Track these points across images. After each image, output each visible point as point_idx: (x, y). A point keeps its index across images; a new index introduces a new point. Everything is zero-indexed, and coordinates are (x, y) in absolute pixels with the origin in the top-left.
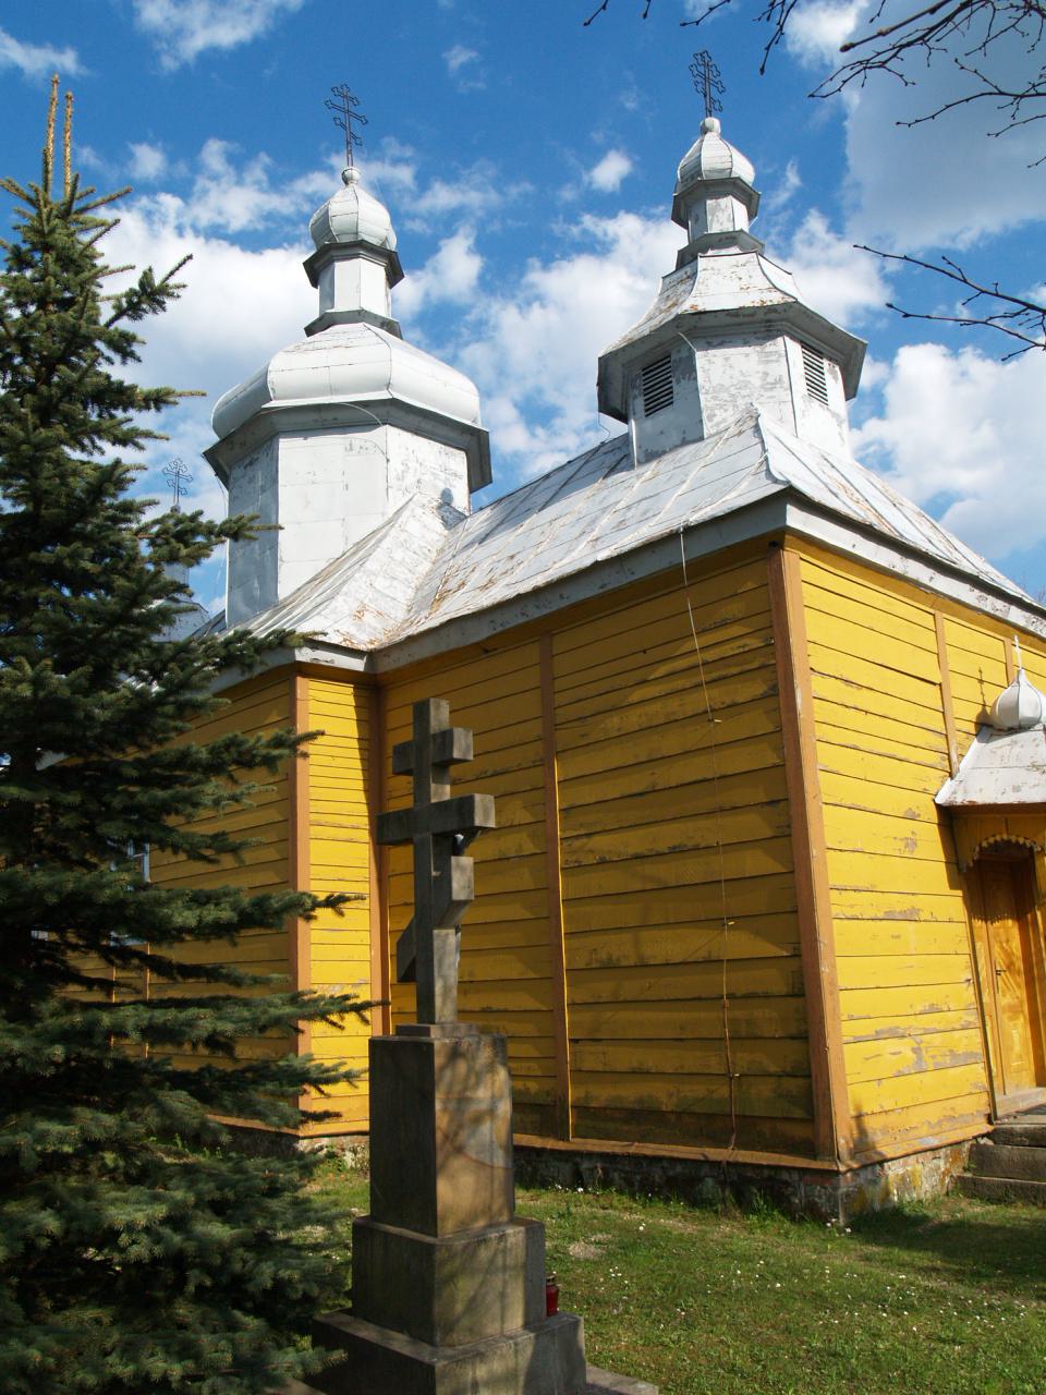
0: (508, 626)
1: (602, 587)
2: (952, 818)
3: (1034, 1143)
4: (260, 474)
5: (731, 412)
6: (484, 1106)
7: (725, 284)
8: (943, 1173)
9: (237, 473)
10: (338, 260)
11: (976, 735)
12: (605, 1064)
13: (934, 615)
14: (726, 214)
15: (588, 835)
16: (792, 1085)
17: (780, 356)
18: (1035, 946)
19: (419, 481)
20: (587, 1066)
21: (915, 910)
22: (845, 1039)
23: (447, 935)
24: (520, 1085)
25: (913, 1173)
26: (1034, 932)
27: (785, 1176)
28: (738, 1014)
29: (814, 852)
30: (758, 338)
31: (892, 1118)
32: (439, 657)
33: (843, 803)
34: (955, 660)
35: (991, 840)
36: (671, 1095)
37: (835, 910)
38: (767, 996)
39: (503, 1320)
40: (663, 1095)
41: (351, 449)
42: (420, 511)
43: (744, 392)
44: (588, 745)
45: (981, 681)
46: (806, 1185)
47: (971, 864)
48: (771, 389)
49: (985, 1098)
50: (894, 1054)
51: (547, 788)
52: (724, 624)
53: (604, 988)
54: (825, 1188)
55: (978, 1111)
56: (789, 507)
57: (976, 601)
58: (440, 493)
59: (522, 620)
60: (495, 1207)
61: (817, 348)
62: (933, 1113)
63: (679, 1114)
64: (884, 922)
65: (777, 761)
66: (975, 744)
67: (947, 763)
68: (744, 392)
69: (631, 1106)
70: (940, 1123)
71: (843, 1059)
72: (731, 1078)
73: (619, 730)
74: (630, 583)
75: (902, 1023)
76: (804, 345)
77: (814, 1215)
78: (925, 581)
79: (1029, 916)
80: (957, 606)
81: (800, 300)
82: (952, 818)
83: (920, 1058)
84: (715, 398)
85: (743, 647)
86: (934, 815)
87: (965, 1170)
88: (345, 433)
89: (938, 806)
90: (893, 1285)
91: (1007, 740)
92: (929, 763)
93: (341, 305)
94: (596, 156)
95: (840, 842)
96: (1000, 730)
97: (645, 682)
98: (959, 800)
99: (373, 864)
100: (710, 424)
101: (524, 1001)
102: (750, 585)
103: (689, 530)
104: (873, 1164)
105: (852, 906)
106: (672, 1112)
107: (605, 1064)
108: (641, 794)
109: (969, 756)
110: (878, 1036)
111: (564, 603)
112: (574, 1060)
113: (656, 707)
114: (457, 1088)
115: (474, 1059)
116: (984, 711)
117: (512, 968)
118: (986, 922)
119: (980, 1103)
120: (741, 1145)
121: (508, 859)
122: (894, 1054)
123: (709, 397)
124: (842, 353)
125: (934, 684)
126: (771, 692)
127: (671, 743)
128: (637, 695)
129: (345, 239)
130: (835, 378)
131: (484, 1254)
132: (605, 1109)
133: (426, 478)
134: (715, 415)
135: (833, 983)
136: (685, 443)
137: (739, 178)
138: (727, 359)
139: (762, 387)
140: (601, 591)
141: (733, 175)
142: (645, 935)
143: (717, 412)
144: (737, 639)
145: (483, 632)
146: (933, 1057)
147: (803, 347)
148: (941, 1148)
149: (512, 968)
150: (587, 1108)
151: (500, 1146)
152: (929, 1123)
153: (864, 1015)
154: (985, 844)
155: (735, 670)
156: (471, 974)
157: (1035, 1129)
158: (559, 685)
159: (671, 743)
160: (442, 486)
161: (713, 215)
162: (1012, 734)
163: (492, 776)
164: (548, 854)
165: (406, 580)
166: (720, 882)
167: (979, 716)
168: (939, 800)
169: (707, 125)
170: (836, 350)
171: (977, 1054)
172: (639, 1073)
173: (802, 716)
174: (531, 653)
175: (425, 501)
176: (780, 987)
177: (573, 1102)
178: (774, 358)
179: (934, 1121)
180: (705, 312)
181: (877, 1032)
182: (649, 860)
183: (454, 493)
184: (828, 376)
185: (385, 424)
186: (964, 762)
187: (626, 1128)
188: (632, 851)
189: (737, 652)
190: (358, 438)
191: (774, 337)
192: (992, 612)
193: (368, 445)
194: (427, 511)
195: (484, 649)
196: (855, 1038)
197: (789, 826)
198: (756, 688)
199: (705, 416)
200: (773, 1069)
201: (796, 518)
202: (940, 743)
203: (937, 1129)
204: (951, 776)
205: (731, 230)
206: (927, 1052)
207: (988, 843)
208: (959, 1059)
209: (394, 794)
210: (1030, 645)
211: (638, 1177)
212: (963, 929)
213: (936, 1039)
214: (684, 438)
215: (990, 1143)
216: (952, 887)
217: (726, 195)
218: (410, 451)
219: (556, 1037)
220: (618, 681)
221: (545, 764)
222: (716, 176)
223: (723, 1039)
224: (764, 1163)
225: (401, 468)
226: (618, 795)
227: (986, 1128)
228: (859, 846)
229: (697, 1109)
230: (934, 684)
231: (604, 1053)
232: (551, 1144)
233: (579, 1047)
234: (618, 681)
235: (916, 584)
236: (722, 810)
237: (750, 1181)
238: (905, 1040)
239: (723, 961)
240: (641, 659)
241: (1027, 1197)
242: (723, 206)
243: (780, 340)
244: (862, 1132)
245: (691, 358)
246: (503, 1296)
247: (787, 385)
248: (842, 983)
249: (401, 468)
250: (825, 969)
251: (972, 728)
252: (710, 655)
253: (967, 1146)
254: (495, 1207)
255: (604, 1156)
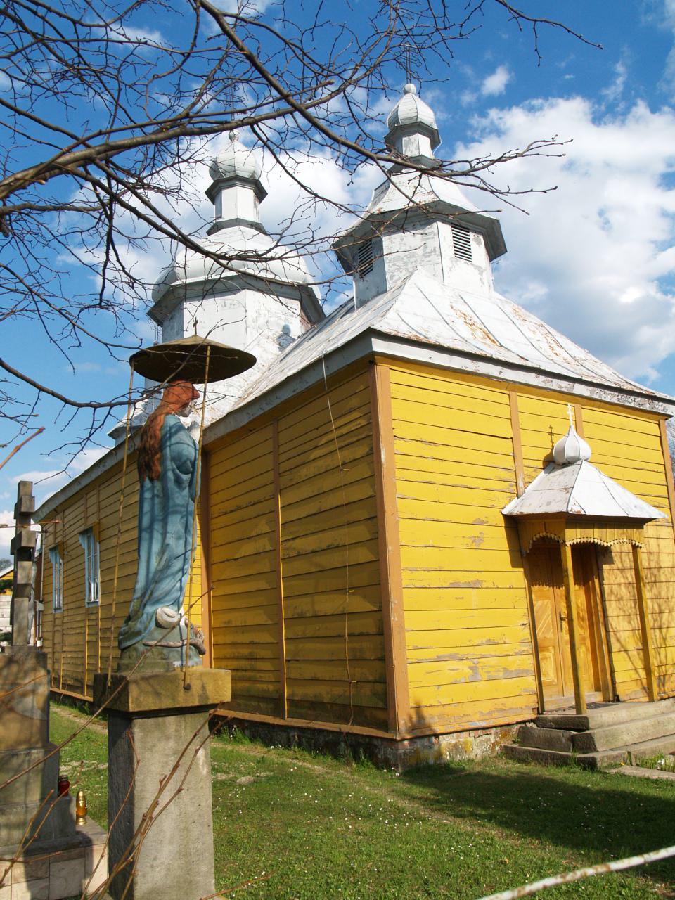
0: (256, 416)
1: (294, 391)
2: (515, 524)
3: (557, 727)
4: (176, 324)
5: (404, 272)
6: (29, 687)
7: (408, 190)
8: (493, 744)
9: (166, 323)
10: (224, 189)
11: (543, 469)
12: (301, 675)
13: (509, 395)
14: (414, 145)
15: (293, 539)
16: (379, 687)
17: (435, 235)
18: (594, 602)
19: (267, 322)
20: (293, 676)
21: (478, 581)
22: (410, 661)
23: (23, 601)
24: (240, 685)
25: (465, 743)
26: (593, 593)
27: (375, 742)
28: (356, 645)
29: (390, 548)
30: (421, 225)
31: (448, 709)
32: (228, 435)
33: (418, 517)
34: (524, 421)
35: (538, 536)
36: (328, 693)
37: (405, 583)
38: (368, 635)
39: (26, 796)
40: (324, 693)
41: (225, 306)
42: (264, 340)
43: (412, 260)
44: (293, 485)
45: (551, 434)
46: (384, 747)
47: (528, 551)
48: (429, 256)
49: (534, 698)
50: (453, 670)
51: (275, 512)
52: (350, 411)
53: (299, 630)
54: (392, 749)
55: (526, 706)
56: (373, 339)
57: (543, 383)
58: (282, 327)
59: (261, 412)
60: (33, 740)
61: (466, 226)
62: (486, 707)
63: (332, 704)
64: (450, 589)
65: (372, 493)
66: (542, 474)
67: (515, 488)
68: (412, 260)
69: (310, 699)
70: (490, 713)
71: (406, 673)
72: (351, 683)
73: (306, 476)
74: (307, 388)
75: (461, 652)
76: (453, 225)
77: (384, 764)
78: (496, 374)
79: (590, 583)
80: (527, 387)
81: (443, 198)
82: (515, 524)
83: (476, 673)
84: (394, 265)
85: (359, 424)
86: (502, 521)
87: (514, 742)
88: (221, 296)
89: (505, 516)
90: (293, 798)
91: (560, 471)
92: (498, 489)
93: (226, 216)
94: (491, 70)
95: (413, 541)
96: (559, 465)
97: (317, 447)
98: (516, 512)
99: (203, 559)
100: (391, 282)
101: (266, 637)
102: (362, 387)
103: (328, 356)
104: (429, 736)
105: (421, 580)
106: (328, 703)
107: (301, 675)
108: (315, 514)
109: (535, 483)
110: (439, 659)
111: (278, 401)
112: (288, 672)
113: (321, 462)
114: (11, 678)
115: (23, 664)
116: (552, 453)
117: (259, 618)
118: (553, 587)
119: (533, 701)
120: (355, 723)
121: (260, 553)
122: (453, 670)
123: (391, 264)
124: (484, 227)
125: (508, 439)
126: (370, 452)
127: (327, 484)
128: (313, 457)
129: (228, 175)
130: (479, 243)
131: (15, 762)
132: (301, 701)
133: (272, 319)
134: (394, 276)
135: (401, 626)
136: (378, 294)
137: (421, 122)
138: (402, 240)
139: (423, 255)
140: (295, 393)
141: (419, 120)
142: (317, 598)
143: (396, 273)
144: (355, 420)
145: (244, 420)
146: (488, 672)
147: (452, 227)
148: (491, 728)
149: (259, 618)
150: (293, 700)
151: (39, 708)
152: (482, 712)
153: (429, 646)
154: (534, 539)
155: (355, 439)
156: (245, 622)
157: (558, 718)
158: (282, 449)
159: (327, 484)
160: (283, 324)
161: (406, 147)
162: (563, 468)
163: (254, 504)
164: (275, 550)
165: (240, 386)
166: (346, 566)
167: (547, 457)
168: (505, 512)
169: (407, 89)
170: (481, 226)
171: (528, 671)
172: (315, 680)
173: (385, 466)
174: (268, 432)
175: (271, 334)
176: (373, 630)
177: (289, 696)
178: (431, 236)
179: (486, 711)
180: (387, 212)
181: (438, 657)
182: (318, 553)
183: (291, 327)
184: (473, 245)
185: (244, 289)
186: (530, 487)
187: (309, 712)
188: (310, 549)
189: (356, 427)
190: (229, 299)
191: (431, 223)
192: (558, 389)
193: (235, 302)
194: (270, 341)
195: (249, 429)
196: (418, 660)
197: (377, 533)
198: (361, 450)
199: (388, 277)
200: (371, 678)
201: (378, 346)
202: (511, 476)
203: (487, 717)
204: (518, 496)
205: (418, 155)
206: (482, 669)
207: (536, 538)
208: (520, 673)
209: (214, 516)
210: (599, 407)
211: (313, 741)
212: (523, 593)
213: (493, 661)
214: (378, 291)
215: (535, 726)
216: (514, 565)
217: (414, 133)
218: (261, 303)
219: (278, 657)
220: (306, 447)
221: (274, 497)
222: (408, 122)
223: (345, 660)
224: (365, 734)
225: (256, 315)
226: (305, 515)
227: (534, 716)
228: (430, 543)
229: (339, 701)
230: (508, 439)
231: (300, 668)
232: (277, 721)
233: (291, 664)
234: (306, 447)
235: (488, 377)
236: (349, 523)
237: (359, 744)
238: (463, 662)
239: (345, 614)
240: (315, 434)
241: (537, 760)
242: (413, 140)
243: (435, 224)
244: (421, 717)
245: (381, 241)
246: (27, 784)
247: (438, 253)
248: (407, 626)
249: (256, 315)
250: (394, 618)
251: (540, 465)
252: (344, 430)
253: (516, 727)
254: (33, 740)
255: (299, 728)
